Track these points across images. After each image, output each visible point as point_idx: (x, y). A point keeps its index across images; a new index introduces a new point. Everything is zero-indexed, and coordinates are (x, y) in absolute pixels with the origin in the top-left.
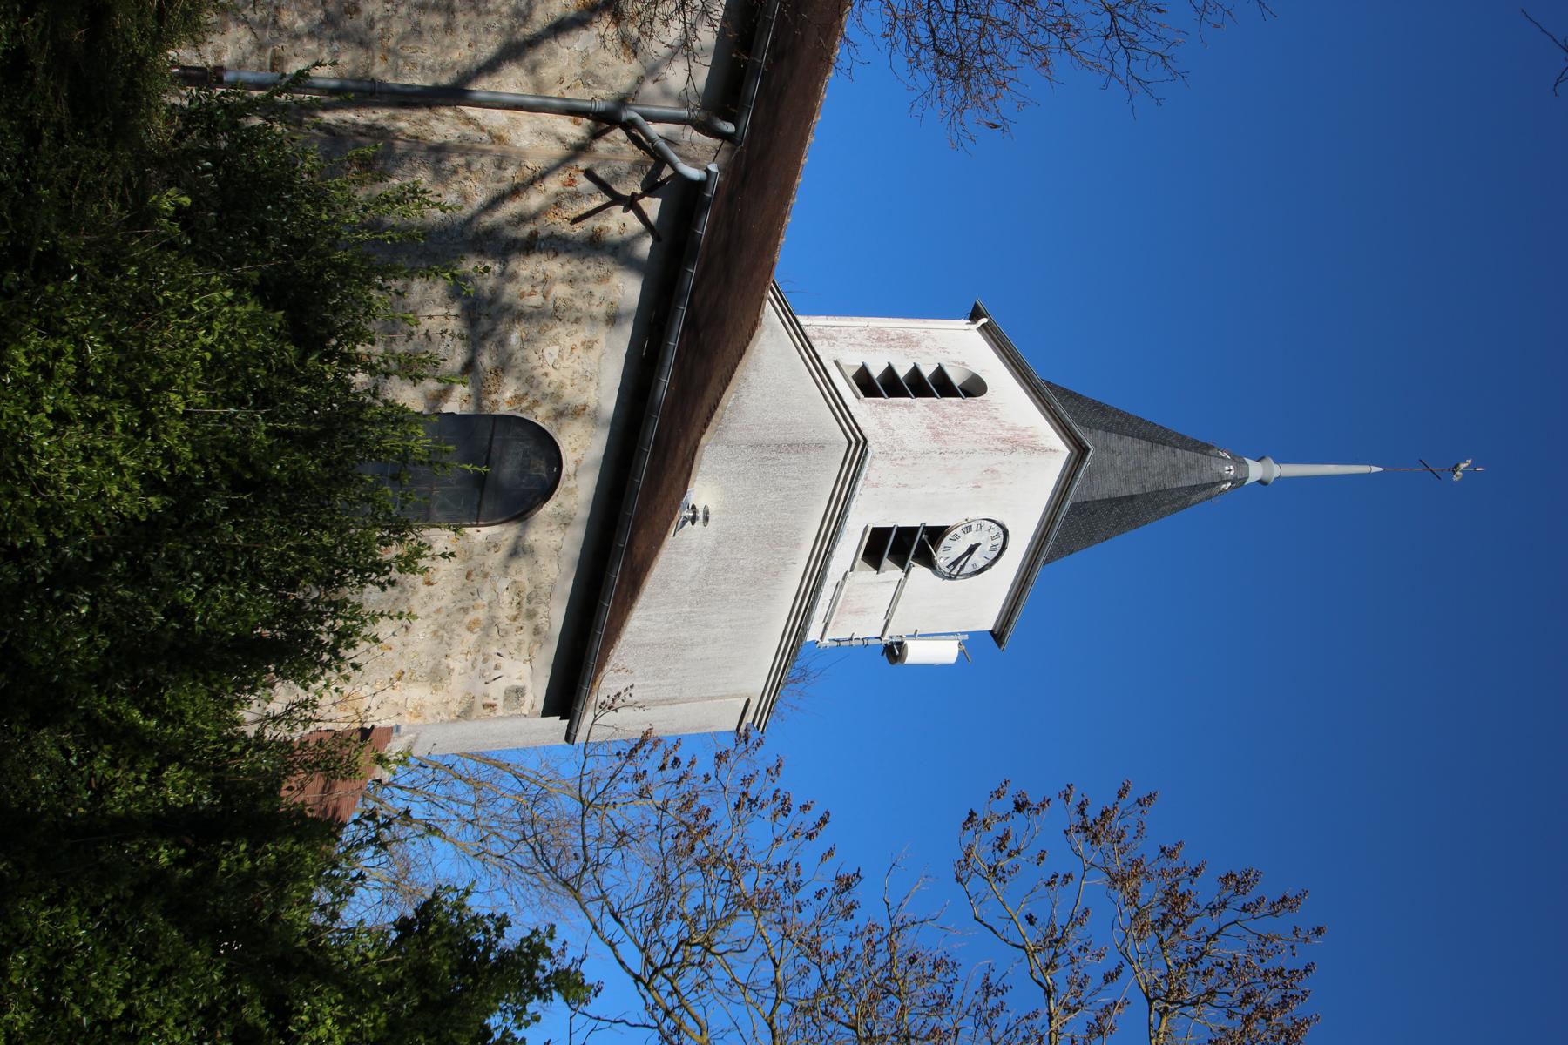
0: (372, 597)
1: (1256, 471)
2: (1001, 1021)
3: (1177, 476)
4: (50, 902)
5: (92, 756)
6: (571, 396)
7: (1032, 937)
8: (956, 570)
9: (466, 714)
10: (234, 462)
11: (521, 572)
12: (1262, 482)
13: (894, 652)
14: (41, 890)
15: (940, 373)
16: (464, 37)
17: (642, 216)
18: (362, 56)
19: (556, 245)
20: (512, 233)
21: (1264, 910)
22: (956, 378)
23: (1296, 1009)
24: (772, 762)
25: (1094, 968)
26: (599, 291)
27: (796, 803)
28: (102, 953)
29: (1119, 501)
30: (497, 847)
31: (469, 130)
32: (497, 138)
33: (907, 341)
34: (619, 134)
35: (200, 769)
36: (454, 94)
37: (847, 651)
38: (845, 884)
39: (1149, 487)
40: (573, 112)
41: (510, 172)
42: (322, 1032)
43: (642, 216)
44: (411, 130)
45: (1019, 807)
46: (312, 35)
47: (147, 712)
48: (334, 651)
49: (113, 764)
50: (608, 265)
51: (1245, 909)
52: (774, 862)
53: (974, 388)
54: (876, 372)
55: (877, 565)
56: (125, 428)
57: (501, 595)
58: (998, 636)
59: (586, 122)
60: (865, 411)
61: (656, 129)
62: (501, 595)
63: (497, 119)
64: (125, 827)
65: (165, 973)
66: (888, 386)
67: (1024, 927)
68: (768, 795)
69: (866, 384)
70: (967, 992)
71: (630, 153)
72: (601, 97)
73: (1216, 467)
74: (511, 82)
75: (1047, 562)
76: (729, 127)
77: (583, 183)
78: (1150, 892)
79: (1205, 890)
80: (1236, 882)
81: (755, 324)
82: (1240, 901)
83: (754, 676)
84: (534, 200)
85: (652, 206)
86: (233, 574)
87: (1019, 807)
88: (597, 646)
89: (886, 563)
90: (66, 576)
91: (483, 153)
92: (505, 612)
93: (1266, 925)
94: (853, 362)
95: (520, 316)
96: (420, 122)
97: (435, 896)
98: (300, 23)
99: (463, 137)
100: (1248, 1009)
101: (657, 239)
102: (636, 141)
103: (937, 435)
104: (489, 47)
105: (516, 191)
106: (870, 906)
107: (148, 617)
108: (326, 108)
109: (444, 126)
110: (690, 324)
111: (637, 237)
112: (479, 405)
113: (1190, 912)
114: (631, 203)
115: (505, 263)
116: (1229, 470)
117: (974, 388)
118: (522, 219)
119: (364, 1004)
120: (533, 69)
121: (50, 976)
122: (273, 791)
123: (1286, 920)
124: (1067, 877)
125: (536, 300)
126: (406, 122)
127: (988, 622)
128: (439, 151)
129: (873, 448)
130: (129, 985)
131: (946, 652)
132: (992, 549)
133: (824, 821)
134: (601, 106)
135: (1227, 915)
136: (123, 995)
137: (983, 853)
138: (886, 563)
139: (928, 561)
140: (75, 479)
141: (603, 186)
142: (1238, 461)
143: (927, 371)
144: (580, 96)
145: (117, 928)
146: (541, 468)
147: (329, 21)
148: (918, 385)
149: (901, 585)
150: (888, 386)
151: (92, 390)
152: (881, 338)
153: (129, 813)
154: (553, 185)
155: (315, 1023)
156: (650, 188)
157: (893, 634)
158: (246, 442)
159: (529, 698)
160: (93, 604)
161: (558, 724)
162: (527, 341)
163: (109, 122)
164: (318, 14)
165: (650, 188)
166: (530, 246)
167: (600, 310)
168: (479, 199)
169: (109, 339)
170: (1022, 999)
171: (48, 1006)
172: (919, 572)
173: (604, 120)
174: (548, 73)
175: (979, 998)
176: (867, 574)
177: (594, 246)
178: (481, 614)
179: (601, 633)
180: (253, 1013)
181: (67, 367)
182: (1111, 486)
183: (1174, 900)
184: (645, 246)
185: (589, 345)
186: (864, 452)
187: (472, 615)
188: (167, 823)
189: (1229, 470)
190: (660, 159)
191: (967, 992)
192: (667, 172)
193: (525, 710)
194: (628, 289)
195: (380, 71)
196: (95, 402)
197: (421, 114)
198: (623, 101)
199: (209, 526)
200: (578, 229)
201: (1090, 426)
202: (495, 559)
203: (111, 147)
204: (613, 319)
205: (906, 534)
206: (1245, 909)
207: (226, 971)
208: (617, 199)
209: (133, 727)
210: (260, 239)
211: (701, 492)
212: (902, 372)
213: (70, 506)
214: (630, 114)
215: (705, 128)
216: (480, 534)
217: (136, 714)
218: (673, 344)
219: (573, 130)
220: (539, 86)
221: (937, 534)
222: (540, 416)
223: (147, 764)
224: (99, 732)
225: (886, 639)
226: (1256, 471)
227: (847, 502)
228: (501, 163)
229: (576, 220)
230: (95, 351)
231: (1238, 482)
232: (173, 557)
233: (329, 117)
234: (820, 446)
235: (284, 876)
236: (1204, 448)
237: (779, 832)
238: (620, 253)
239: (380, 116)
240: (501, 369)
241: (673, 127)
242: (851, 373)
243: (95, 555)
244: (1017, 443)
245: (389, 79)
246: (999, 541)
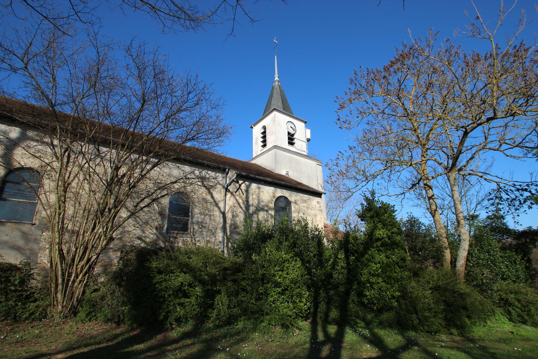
0: (310, 225)
1: (277, 78)
2: (374, 121)
3: (278, 93)
4: (361, 275)
5: (337, 269)
6: (271, 195)
7: (360, 117)
8: (295, 130)
9: (321, 210)
10: (291, 247)
11: (299, 202)
13: (308, 140)
14: (359, 276)
15: (262, 133)
16: (215, 213)
17: (242, 183)
18: (218, 229)
19: (247, 197)
20: (246, 204)
21: (357, 77)
22: (263, 131)
23: (375, 71)
24: (331, 161)
25: (366, 106)
26: (254, 190)
27: (338, 157)
28: (370, 267)
29: (282, 102)
30: (341, 205)
31: (230, 212)
32: (231, 207)
33: (257, 139)
34: (229, 187)
35: (338, 253)
36: (224, 214)
37: (309, 148)
38: (351, 148)
39: (280, 97)
40: (226, 195)
41: (236, 205)
42: (381, 233)
43: (242, 183)
44: (230, 221)
45: (339, 120)
46: (215, 237)
47: (329, 260)
48: (319, 232)
49: (338, 266)
50: (250, 189)
51: (356, 80)
52: (347, 160)
53: (264, 128)
54: (262, 144)
55: (294, 143)
56: (288, 264)
57: (302, 205)
58: (305, 123)
59: (227, 193)
60: (269, 146)
61: (228, 182)
62: (302, 205)
63: (227, 207)
64: (348, 263)
65: (372, 257)
66: (264, 141)
67: (359, 118)
68: (336, 162)
69: (264, 146)
70: (369, 127)
71: (232, 185)
72: (223, 191)
73: (276, 85)
74: (221, 205)
75: (293, 114)
76: (227, 170)
77: (237, 193)
78: (353, 97)
79: (353, 87)
80: (352, 81)
81: (255, 164)
82: (355, 81)
83: (313, 163)
84: (240, 201)
85: (241, 182)
86: (308, 247)
87: (339, 120)
88: (311, 190)
89: (294, 142)
90: (309, 273)
91: (233, 209)
92: (305, 205)
93: (359, 76)
94: (261, 148)
95: (259, 203)
96: (229, 220)
97: (357, 215)
98: (214, 239)
99: (231, 212)
100: (374, 79)
101: (245, 181)
102: (230, 185)
103: (273, 134)
104: (216, 209)
105: (239, 204)
106: (355, 144)
107: (315, 260)
108: (227, 234)
109: (229, 216)
110: (259, 175)
111: (245, 184)
112: (273, 209)
113: (356, 89)
114: (240, 185)
115: (250, 205)
116: (277, 83)
117: (264, 128)
118: (244, 203)
119: (377, 226)
120: (219, 202)
121: (373, 275)
122: (341, 241)
123: (359, 73)
124: (350, 111)
125: (256, 200)
126: (229, 222)
127: (303, 124)
128: (233, 216)
130: (375, 263)
131: (308, 131)
133: (340, 152)
134: (225, 190)
135: (357, 83)
136: (376, 264)
137: (346, 125)
138: (294, 142)
139: (293, 135)
140: (297, 271)
141: (238, 190)
142: (275, 82)
143: (262, 136)
144: (223, 194)
145: (366, 265)
146: (282, 199)
147: (213, 234)
148: (264, 137)
149: (298, 139)
150: (264, 141)
151: (283, 269)
152: (256, 143)
154: (238, 198)
155: (380, 234)
156: (238, 182)
157: (306, 140)
158: (288, 246)
159: (319, 200)
160: (313, 269)
161: (323, 196)
162: (262, 202)
163: (241, 267)
164: (212, 236)
165: (238, 182)
166: (247, 201)
167: (257, 190)
168: (240, 210)
169: (275, 266)
170: (370, 118)
171: (378, 276)
172: (295, 136)
173: (227, 190)
174: (220, 199)
175: (370, 125)
176: (296, 145)
177: (247, 191)
178: (305, 208)
179: (308, 189)
180: (379, 244)
181: (280, 273)
182: (280, 104)
183: (355, 93)
184: (247, 183)
185: (263, 192)
186: (276, 146)
187: (306, 210)
188: (347, 257)
190: (233, 181)
191: (369, 127)
192: (235, 180)
193: (320, 201)
194: (254, 186)
195: (221, 225)
196: (285, 269)
197: (227, 219)
198: (224, 187)
199: (301, 251)
200: (245, 194)
201: (270, 108)
202: (297, 207)
203: (245, 267)
204: (259, 188)
205: (289, 139)
206: (356, 80)
207: (372, 248)
208: (240, 188)
209: (333, 263)
210: (255, 244)
211: (283, 173)
212: (262, 140)
213: (301, 272)
214: (226, 186)
215: (227, 174)
216: (293, 209)
217: (330, 262)
218: (262, 178)
219: (229, 195)
220: (222, 200)
221: (289, 133)
222: (274, 200)
223: (338, 260)
224: (333, 268)
225: (306, 141)
226: (277, 78)
227: (284, 149)
228: (235, 207)
229: (243, 194)
230: (277, 268)
231: (279, 82)
232: (306, 256)
233: (228, 234)
234: (275, 153)
235: (355, 239)
236: (273, 88)
237: (342, 159)
238: (248, 187)
239: (228, 226)
240: (267, 206)
241: (227, 179)
242: (262, 148)
243: (306, 268)
244: (274, 120)
245: (222, 224)
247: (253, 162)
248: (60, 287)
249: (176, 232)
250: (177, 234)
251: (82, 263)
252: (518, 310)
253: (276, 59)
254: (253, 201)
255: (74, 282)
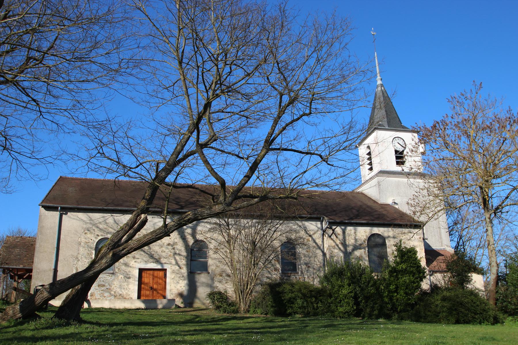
12: (381, 79)
19: (344, 237)
55: (404, 162)
81: (362, 194)
85: (334, 227)
89: (404, 160)
94: (368, 172)
116: (379, 88)
117: (368, 147)
129: (380, 169)
132: (399, 139)
138: (404, 160)
139: (402, 153)
142: (377, 87)
153: (464, 287)
189: (379, 88)
205: (397, 158)
211: (390, 201)
221: (396, 152)
226: (379, 82)
231: (382, 85)
238: (344, 232)
246: (397, 138)
247: (360, 190)
248: (241, 300)
249: (290, 272)
250: (291, 273)
251: (248, 290)
252: (95, 200)
253: (376, 60)
254: (350, 241)
255: (246, 298)
